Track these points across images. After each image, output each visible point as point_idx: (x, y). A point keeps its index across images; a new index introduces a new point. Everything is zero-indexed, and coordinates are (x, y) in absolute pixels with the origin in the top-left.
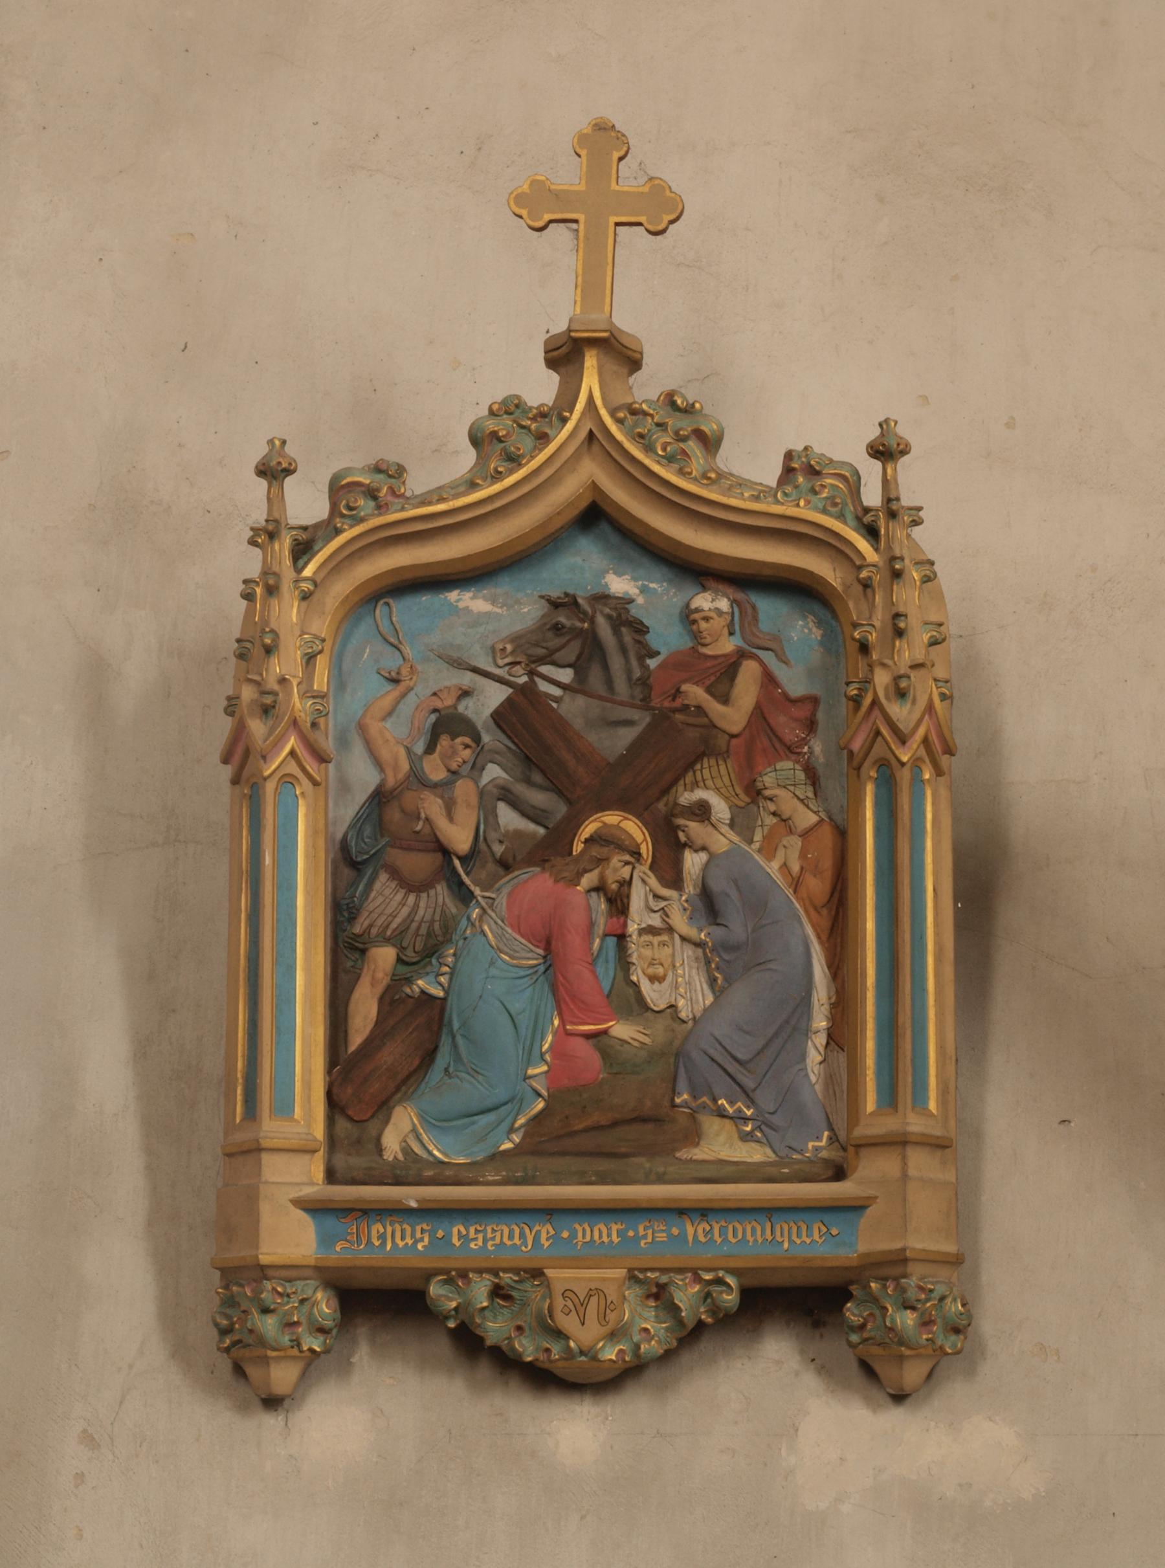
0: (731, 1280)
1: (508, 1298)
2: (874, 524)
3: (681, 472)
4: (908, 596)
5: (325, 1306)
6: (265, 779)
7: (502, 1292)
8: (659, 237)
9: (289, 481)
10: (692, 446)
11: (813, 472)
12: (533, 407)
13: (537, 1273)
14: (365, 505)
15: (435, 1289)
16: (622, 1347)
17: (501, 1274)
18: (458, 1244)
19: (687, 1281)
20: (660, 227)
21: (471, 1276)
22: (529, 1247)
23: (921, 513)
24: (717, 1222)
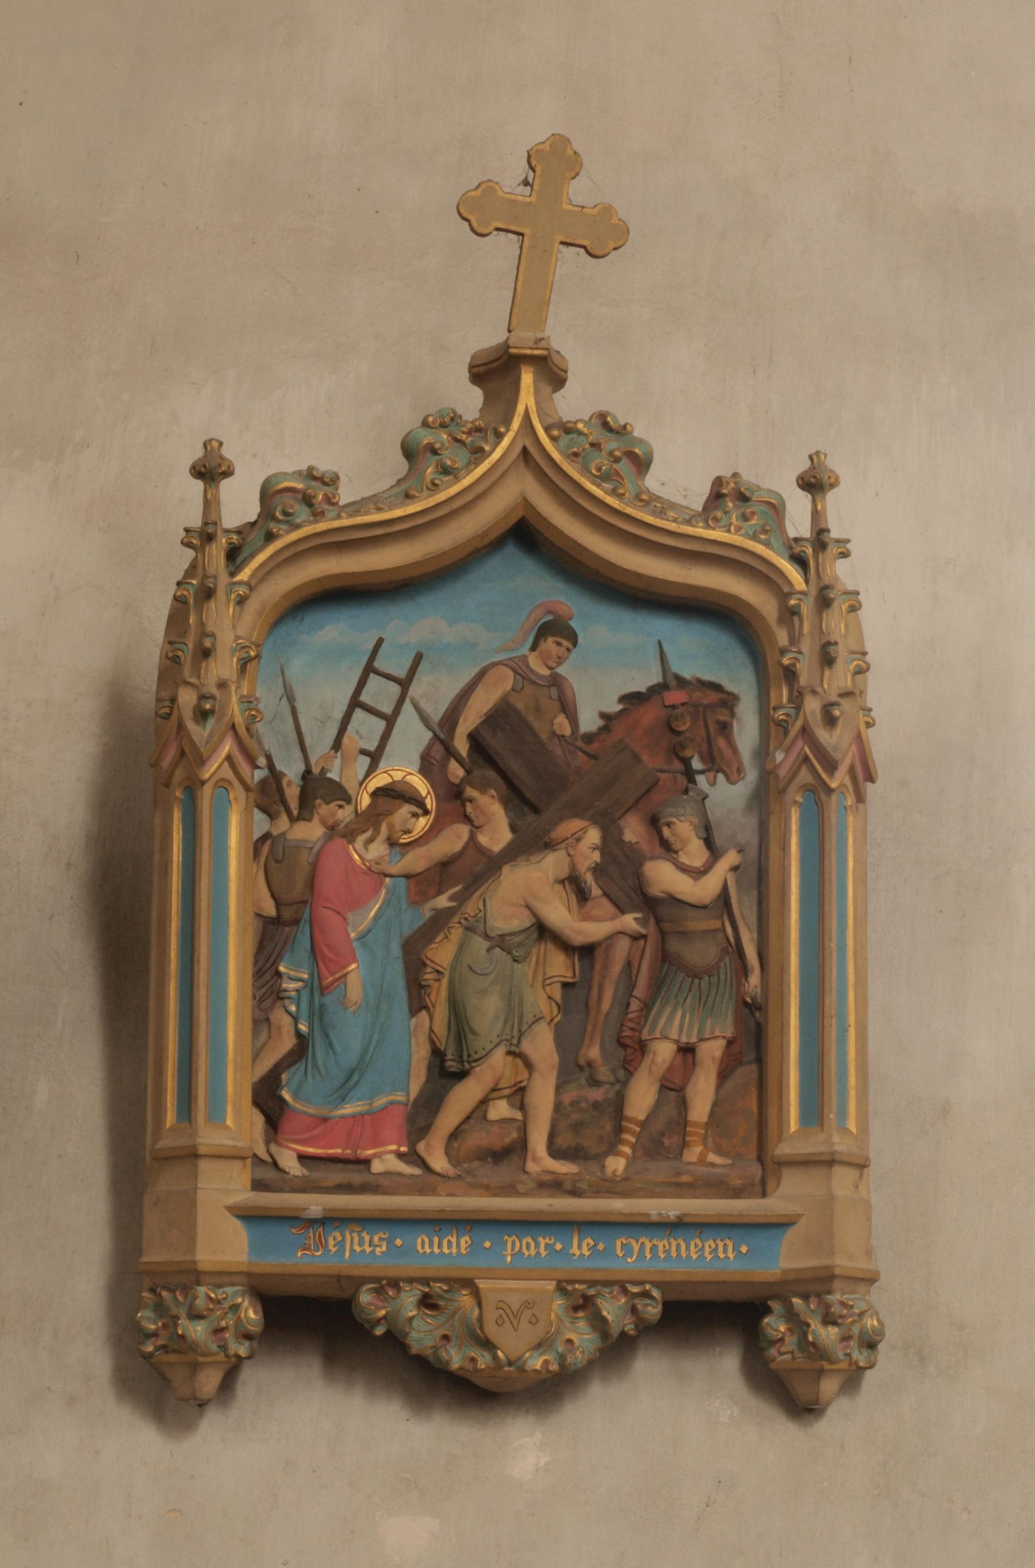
0: (656, 1293)
1: (434, 1307)
2: (803, 554)
3: (614, 492)
4: (835, 623)
5: (252, 1315)
6: (203, 783)
7: (430, 1301)
8: (589, 258)
9: (225, 484)
10: (624, 467)
11: (743, 498)
12: (468, 421)
13: (468, 1283)
14: (302, 513)
15: (365, 1297)
16: (546, 1357)
17: (431, 1284)
18: (620, 1255)
19: (615, 1293)
20: (485, 231)
21: (402, 1285)
22: (633, 1260)
23: (849, 546)
24: (721, 1240)
